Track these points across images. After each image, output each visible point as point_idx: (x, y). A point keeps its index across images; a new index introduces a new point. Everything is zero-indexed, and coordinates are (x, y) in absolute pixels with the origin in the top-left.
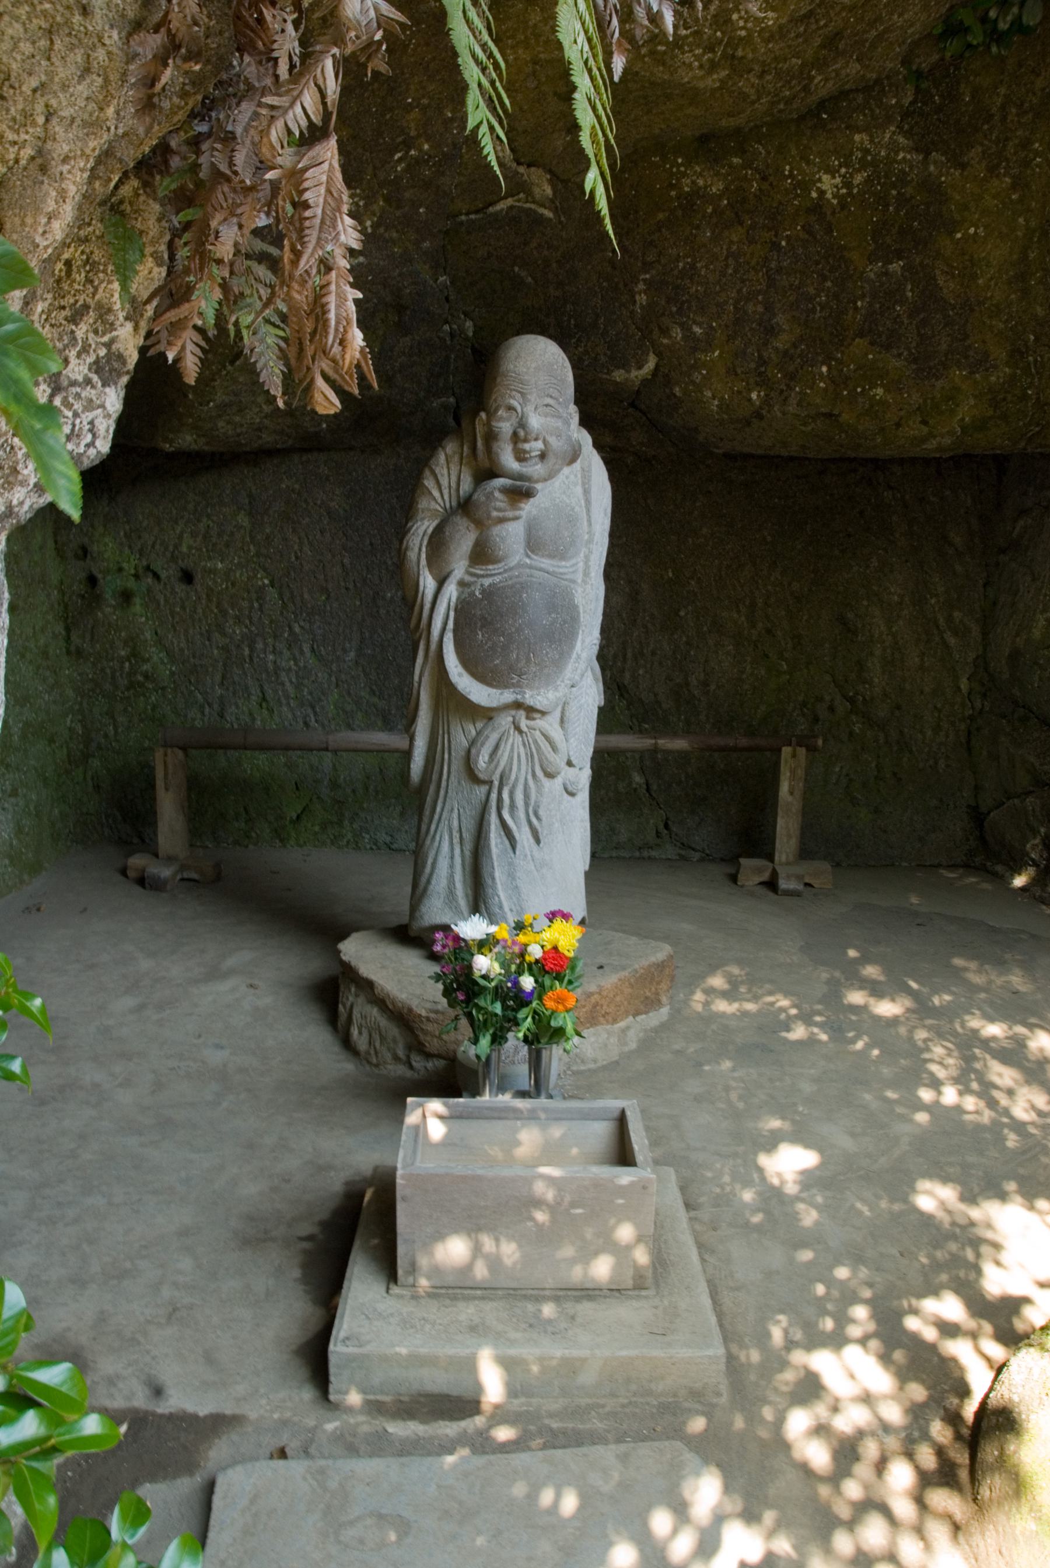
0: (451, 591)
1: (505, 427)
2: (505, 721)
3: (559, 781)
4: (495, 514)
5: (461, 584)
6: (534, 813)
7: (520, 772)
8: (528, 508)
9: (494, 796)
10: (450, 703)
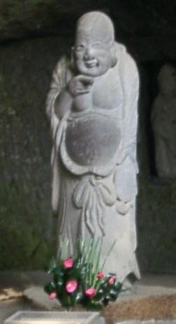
0: (64, 124)
1: (80, 54)
2: (86, 179)
3: (114, 207)
4: (78, 91)
5: (69, 121)
6: (101, 221)
7: (93, 202)
8: (91, 89)
9: (83, 214)
10: (65, 173)
